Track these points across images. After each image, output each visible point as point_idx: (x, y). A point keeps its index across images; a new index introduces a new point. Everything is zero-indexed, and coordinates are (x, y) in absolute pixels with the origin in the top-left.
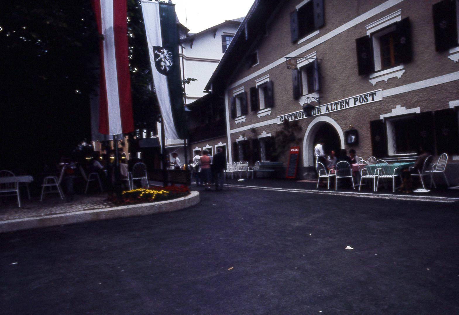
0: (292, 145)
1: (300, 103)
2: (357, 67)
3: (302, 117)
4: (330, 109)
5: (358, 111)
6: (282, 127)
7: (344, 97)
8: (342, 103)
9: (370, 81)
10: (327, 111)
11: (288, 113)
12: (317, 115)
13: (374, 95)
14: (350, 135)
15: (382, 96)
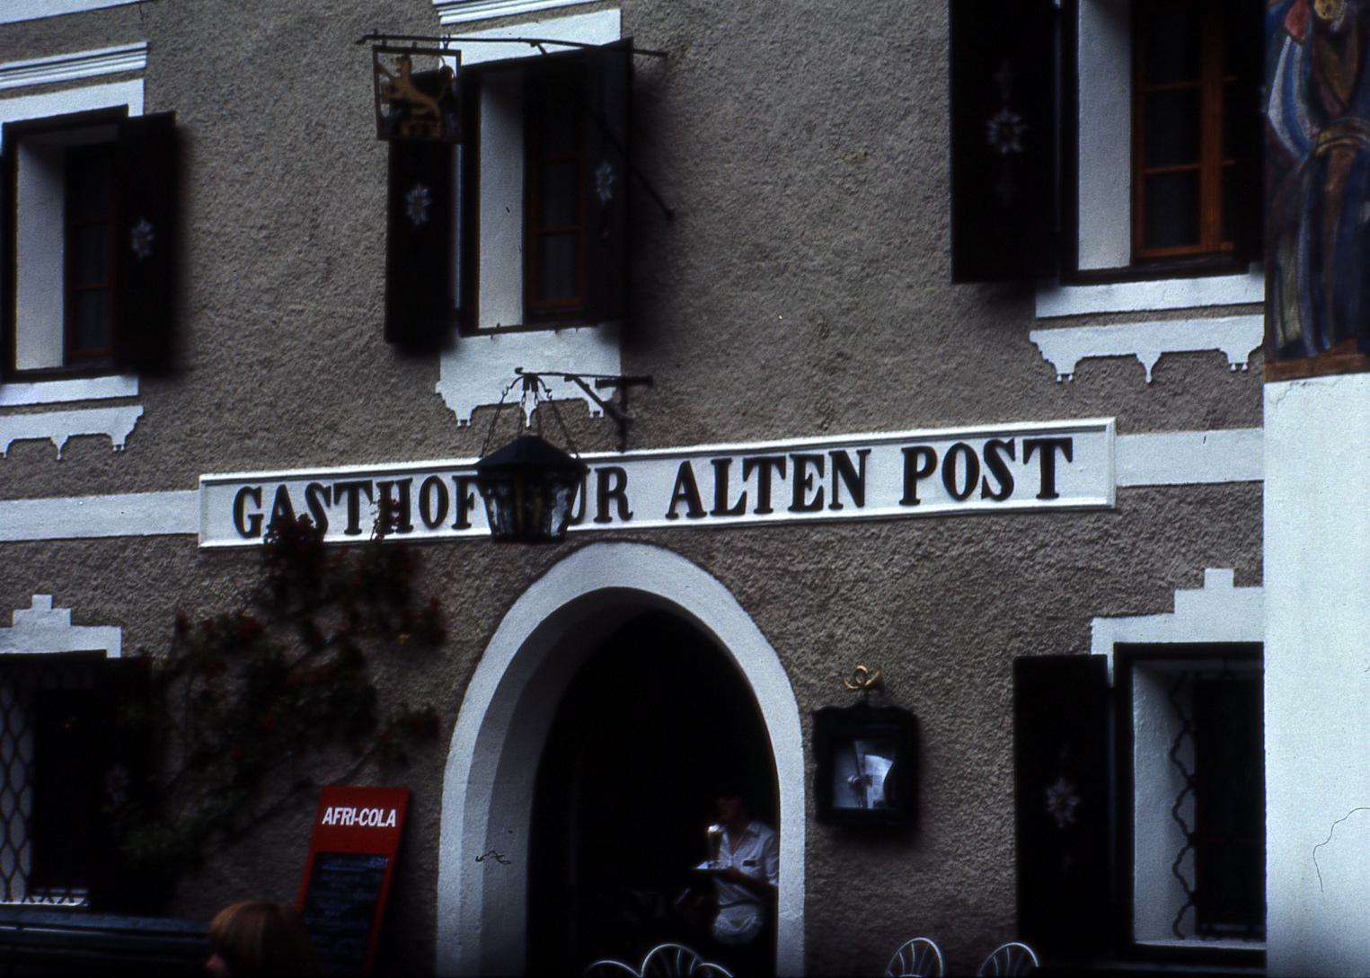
0: (333, 766)
1: (439, 388)
2: (944, 199)
3: (452, 518)
4: (708, 502)
5: (927, 556)
6: (251, 579)
7: (827, 420)
8: (810, 469)
9: (1036, 336)
10: (683, 508)
11: (318, 464)
12: (589, 525)
13: (1059, 456)
14: (859, 746)
15: (1115, 477)
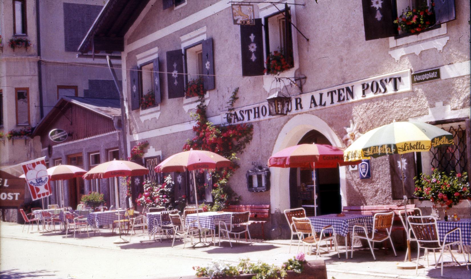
4: (318, 103)
10: (313, 105)
